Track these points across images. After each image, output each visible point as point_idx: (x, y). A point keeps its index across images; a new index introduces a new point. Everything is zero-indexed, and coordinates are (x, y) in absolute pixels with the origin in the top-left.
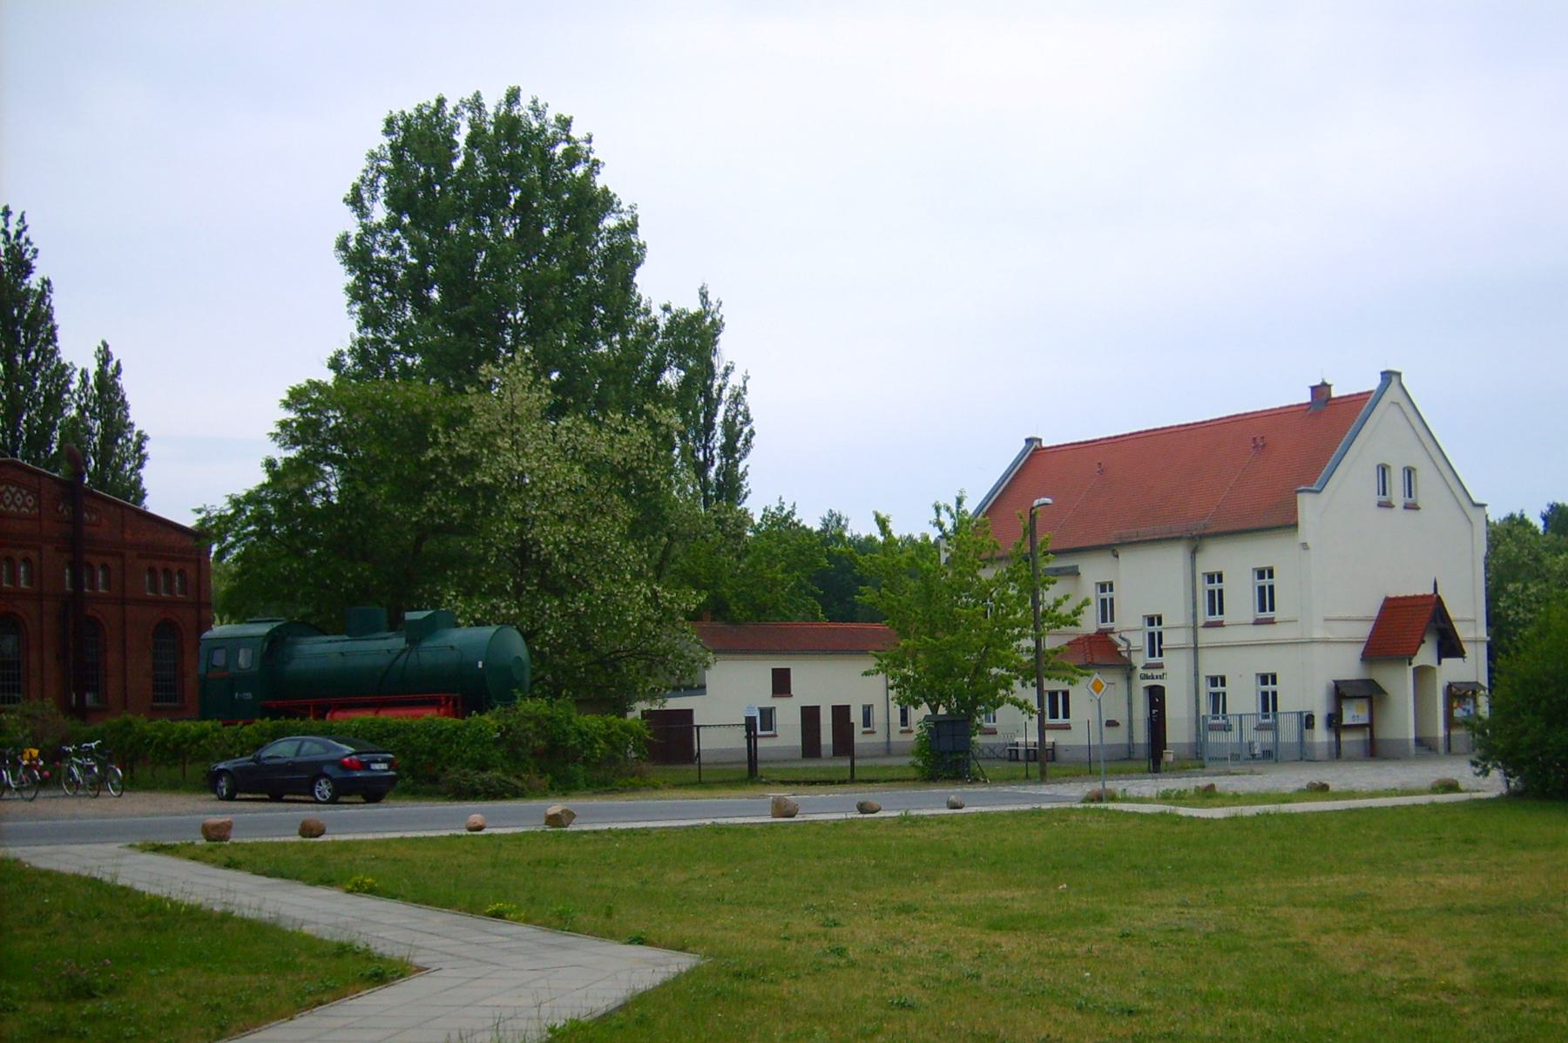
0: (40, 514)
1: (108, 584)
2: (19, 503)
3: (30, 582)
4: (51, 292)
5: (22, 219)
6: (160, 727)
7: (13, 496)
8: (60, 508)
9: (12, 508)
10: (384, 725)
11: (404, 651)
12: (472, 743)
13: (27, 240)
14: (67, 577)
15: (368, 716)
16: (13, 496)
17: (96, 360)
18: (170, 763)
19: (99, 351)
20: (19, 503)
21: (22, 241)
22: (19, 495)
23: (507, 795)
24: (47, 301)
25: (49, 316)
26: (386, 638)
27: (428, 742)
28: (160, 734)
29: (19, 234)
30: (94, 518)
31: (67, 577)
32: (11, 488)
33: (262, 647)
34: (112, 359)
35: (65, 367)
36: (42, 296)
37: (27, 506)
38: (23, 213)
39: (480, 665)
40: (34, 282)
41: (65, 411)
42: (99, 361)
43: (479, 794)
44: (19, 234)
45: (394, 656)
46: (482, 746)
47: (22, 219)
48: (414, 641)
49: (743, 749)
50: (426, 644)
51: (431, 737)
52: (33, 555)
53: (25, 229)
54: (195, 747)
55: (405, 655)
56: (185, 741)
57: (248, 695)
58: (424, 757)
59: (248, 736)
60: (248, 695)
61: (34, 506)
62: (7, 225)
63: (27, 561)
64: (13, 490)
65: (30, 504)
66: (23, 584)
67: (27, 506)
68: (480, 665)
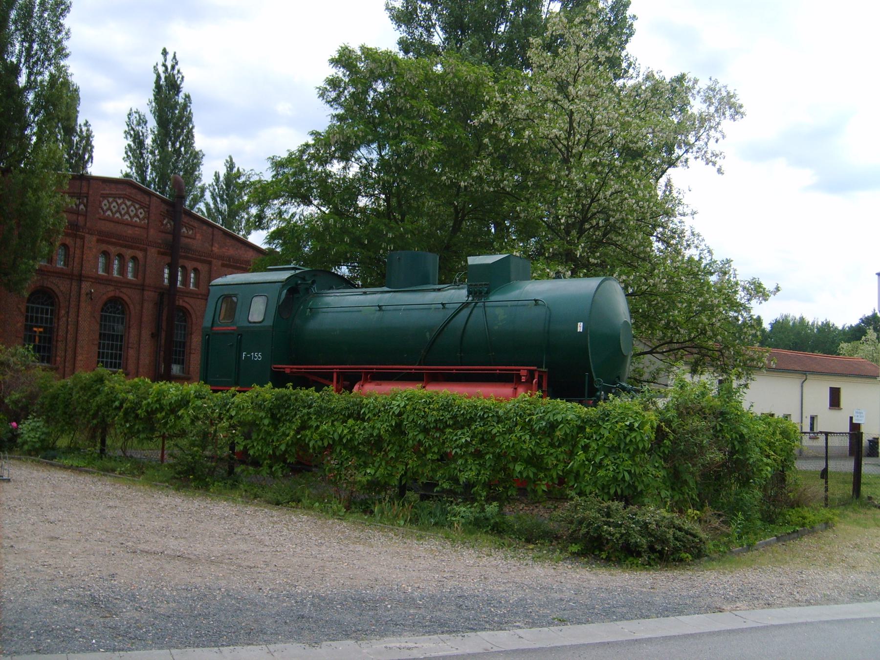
0: (148, 223)
1: (197, 284)
2: (132, 214)
3: (136, 275)
4: (190, 103)
5: (174, 57)
6: (135, 387)
7: (128, 207)
8: (165, 222)
9: (127, 217)
10: (447, 407)
11: (465, 305)
12: (614, 449)
13: (179, 71)
14: (166, 276)
15: (414, 389)
16: (128, 207)
17: (225, 168)
18: (142, 436)
19: (227, 161)
20: (132, 214)
21: (176, 72)
22: (132, 208)
23: (684, 555)
24: (189, 109)
25: (189, 119)
26: (439, 290)
27: (529, 444)
28: (130, 397)
29: (173, 68)
30: (190, 232)
31: (166, 276)
32: (127, 202)
33: (280, 294)
34: (235, 167)
35: (197, 153)
36: (185, 107)
37: (138, 217)
38: (175, 53)
39: (580, 327)
40: (181, 99)
41: (197, 183)
42: (227, 168)
43: (639, 555)
44: (173, 68)
45: (450, 312)
46: (632, 457)
47: (174, 57)
48: (478, 293)
49: (821, 447)
50: (492, 298)
51: (533, 433)
52: (140, 255)
53: (177, 63)
54: (172, 417)
55: (465, 312)
56: (162, 409)
57: (258, 356)
58: (518, 468)
59: (239, 408)
60: (258, 356)
61: (143, 219)
62: (165, 61)
63: (134, 259)
64: (129, 203)
65: (141, 216)
66: (130, 276)
67: (138, 217)
68: (580, 327)
